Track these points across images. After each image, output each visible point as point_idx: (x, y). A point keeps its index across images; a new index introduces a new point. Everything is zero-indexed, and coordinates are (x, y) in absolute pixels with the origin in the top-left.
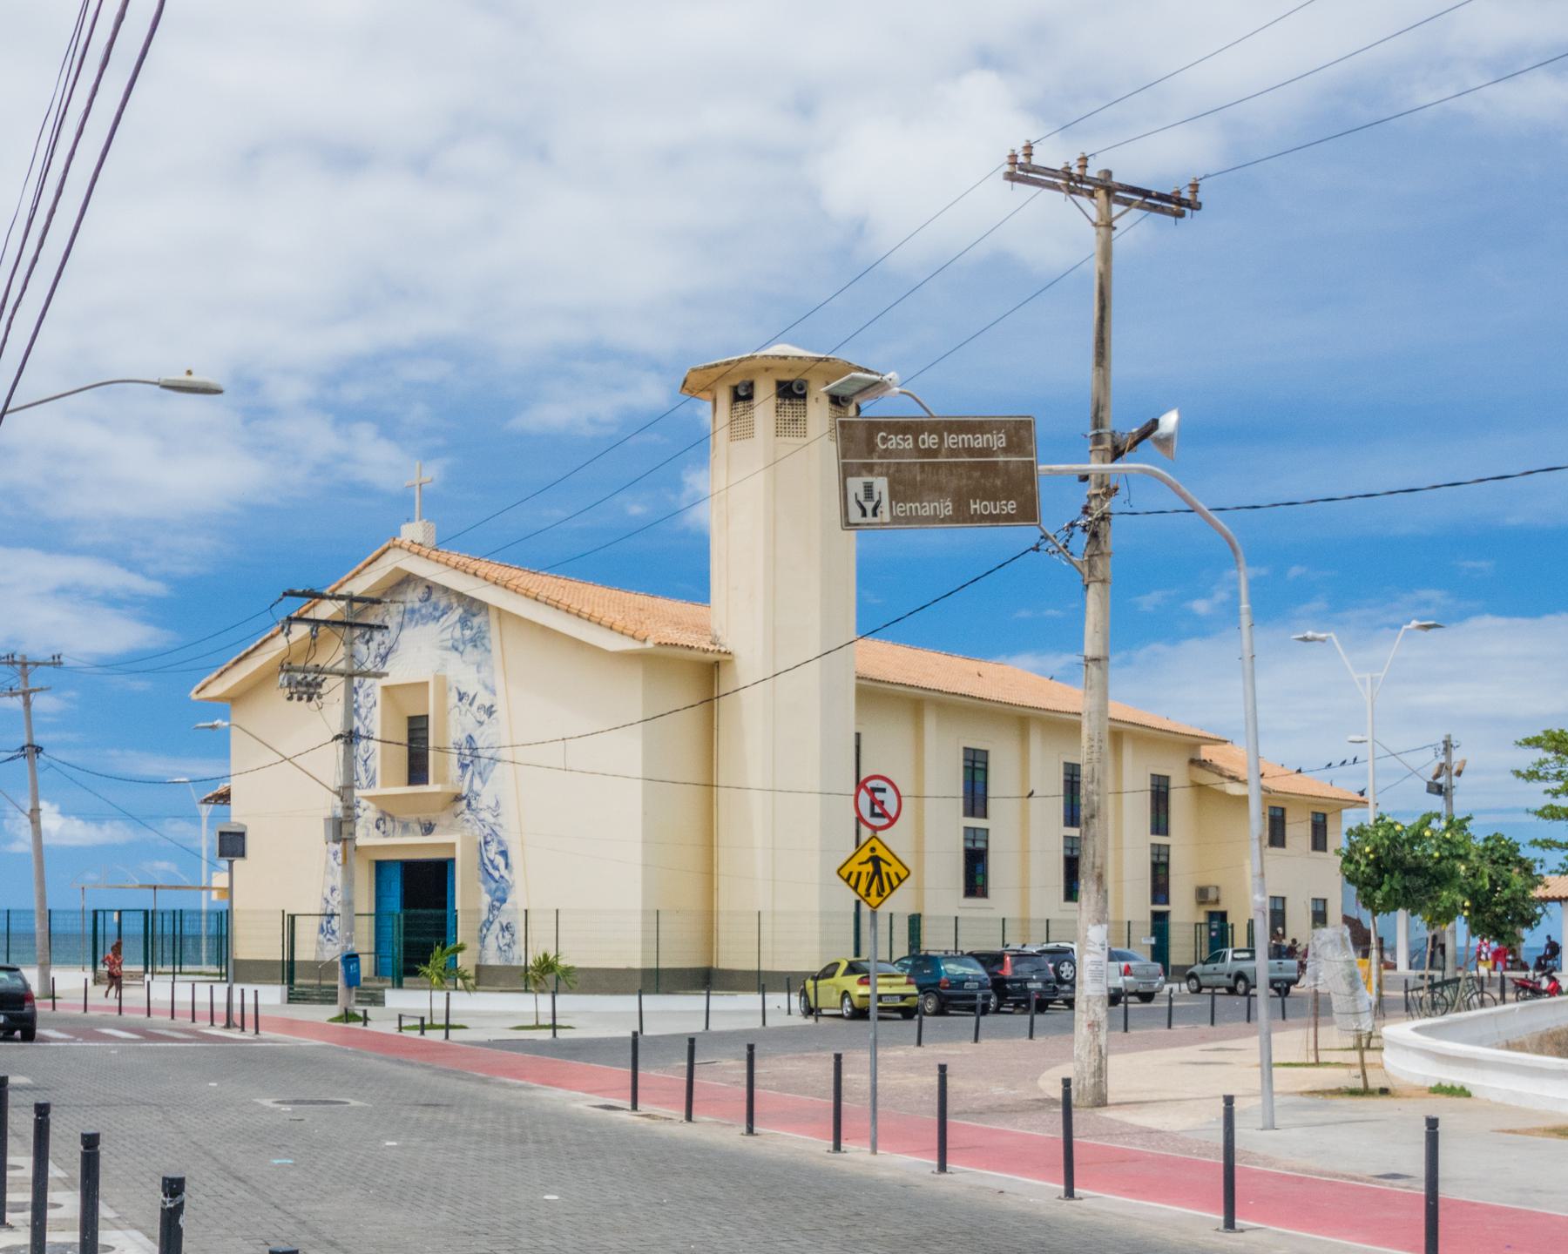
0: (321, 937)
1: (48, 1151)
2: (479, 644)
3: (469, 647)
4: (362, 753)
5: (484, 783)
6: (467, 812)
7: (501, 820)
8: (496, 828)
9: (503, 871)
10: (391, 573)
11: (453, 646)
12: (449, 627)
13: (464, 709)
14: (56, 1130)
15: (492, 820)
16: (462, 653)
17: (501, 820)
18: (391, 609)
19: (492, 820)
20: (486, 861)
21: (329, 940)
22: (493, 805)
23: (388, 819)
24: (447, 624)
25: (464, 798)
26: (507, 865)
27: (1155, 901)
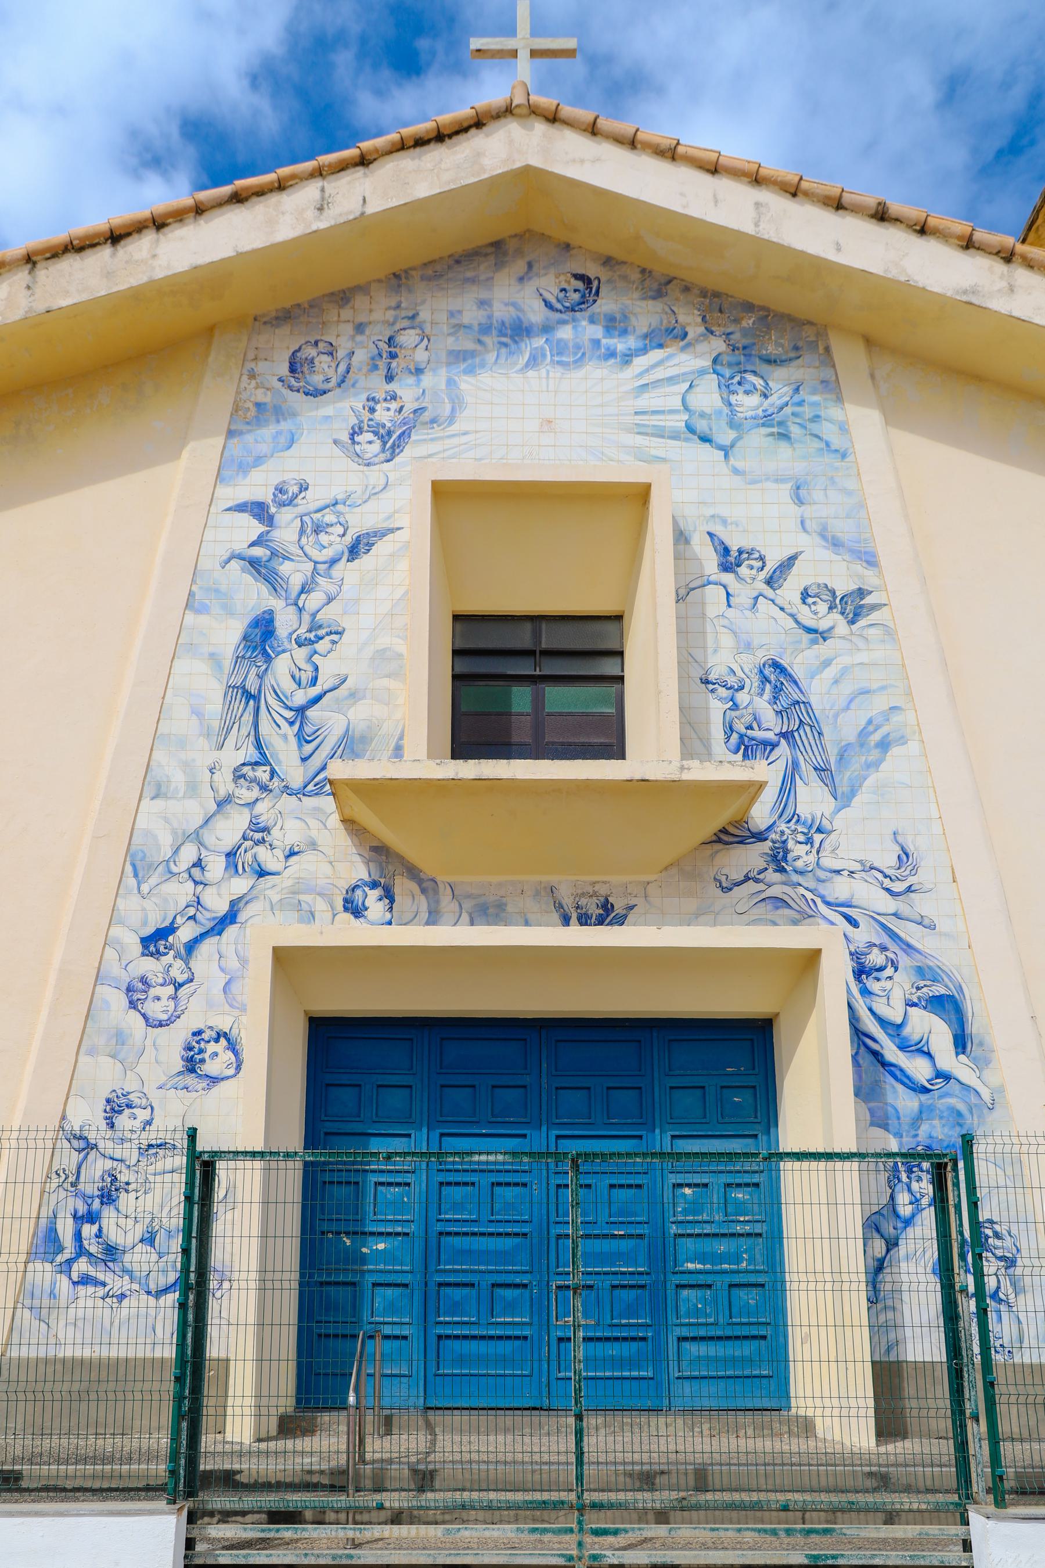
0: (43, 1272)
1: (628, 197)
2: (795, 430)
3: (757, 438)
4: (287, 684)
5: (843, 799)
6: (772, 876)
7: (922, 905)
8: (909, 932)
9: (946, 1057)
10: (495, 183)
11: (690, 429)
12: (671, 380)
13: (743, 595)
14: (665, 322)
15: (886, 904)
16: (726, 451)
17: (922, 905)
18: (424, 315)
19: (886, 904)
20: (871, 1026)
21: (85, 1280)
22: (887, 860)
23: (403, 886)
24: (660, 373)
25: (760, 837)
26: (961, 1042)
27: (186, 1549)
